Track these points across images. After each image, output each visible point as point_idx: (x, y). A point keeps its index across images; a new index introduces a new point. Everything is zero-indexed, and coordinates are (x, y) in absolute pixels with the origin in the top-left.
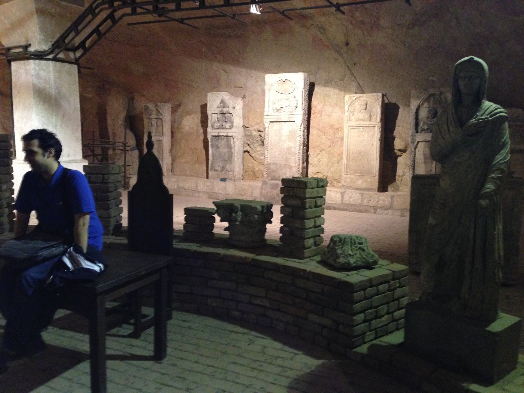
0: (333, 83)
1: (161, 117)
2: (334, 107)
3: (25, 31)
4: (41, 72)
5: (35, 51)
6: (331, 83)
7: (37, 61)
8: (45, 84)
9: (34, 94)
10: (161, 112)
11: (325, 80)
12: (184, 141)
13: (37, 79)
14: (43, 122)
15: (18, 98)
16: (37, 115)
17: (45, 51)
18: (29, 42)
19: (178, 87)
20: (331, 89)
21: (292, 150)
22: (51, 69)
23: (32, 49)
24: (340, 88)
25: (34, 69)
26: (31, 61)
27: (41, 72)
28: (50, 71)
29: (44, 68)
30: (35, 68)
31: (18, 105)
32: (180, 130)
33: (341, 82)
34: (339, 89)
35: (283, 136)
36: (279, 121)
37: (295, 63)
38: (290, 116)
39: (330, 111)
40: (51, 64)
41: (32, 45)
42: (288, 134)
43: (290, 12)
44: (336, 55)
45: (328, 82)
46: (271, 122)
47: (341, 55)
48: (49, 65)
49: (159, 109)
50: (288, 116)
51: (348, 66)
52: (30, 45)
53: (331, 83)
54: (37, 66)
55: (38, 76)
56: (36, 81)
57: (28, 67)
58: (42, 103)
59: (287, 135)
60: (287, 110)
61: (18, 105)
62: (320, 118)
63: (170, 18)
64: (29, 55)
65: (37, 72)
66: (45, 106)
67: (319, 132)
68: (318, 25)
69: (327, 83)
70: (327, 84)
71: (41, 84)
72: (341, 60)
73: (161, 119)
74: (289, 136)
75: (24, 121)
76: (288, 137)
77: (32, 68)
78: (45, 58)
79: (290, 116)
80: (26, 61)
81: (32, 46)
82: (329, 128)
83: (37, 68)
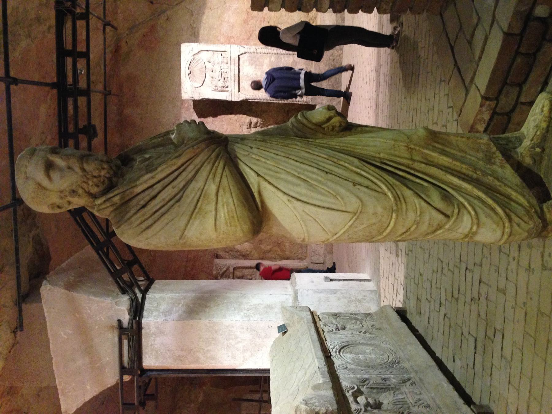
0: (195, 26)
1: (231, 269)
2: (223, 20)
3: (97, 327)
4: (163, 308)
5: (129, 314)
6: (195, 28)
7: (145, 313)
8: (179, 304)
9: (193, 319)
10: (225, 269)
11: (191, 35)
12: (262, 246)
13: (171, 313)
14: (235, 310)
15: (198, 354)
16: (224, 316)
17: (131, 300)
18: (115, 324)
19: (194, 257)
20: (202, 28)
21: (274, 61)
22: (157, 296)
23: (126, 318)
24: (200, 15)
25: (156, 317)
26: (144, 321)
27: (163, 308)
28: (160, 297)
29: (155, 305)
30: (155, 316)
31: (209, 355)
32: (248, 252)
33: (194, 14)
34: (202, 16)
35: (256, 74)
36: (237, 78)
37: (171, 78)
38: (233, 63)
39: (227, 26)
40: (150, 296)
41: (119, 319)
42: (254, 66)
43: (102, 6)
44: (163, 18)
45: (193, 32)
46: (239, 91)
47: (163, 12)
48: (152, 299)
49: (221, 272)
50: (232, 65)
51: (177, 4)
52: (119, 321)
53: (195, 28)
54: (152, 314)
55: (165, 313)
56: (175, 316)
57: (153, 330)
58: (207, 310)
59: (255, 68)
60: (225, 67)
61: (209, 355)
62: (235, 37)
63: (108, 254)
64: (134, 321)
65: (161, 314)
66: (211, 306)
67: (251, 38)
68: (127, 34)
69: (195, 34)
70: (196, 33)
71: (178, 311)
72: (169, 13)
73: (234, 269)
74: (256, 65)
75: (233, 342)
76: (257, 67)
77: (155, 320)
78: (140, 301)
79: (233, 63)
80: (144, 332)
81: (122, 319)
82: (247, 26)
83: (154, 314)
